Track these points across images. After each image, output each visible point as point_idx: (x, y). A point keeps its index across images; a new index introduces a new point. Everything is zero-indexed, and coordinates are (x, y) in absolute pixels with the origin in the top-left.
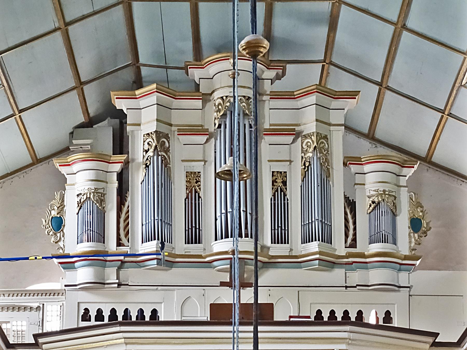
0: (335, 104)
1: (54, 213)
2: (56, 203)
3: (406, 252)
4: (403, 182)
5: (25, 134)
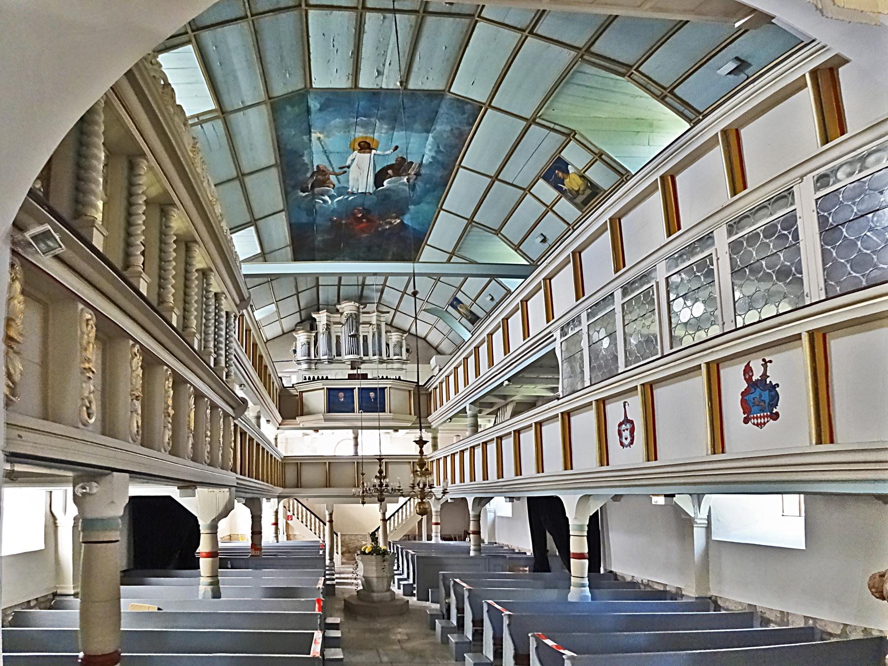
0: (383, 315)
1: (294, 348)
2: (294, 345)
3: (405, 359)
4: (404, 338)
5: (281, 326)
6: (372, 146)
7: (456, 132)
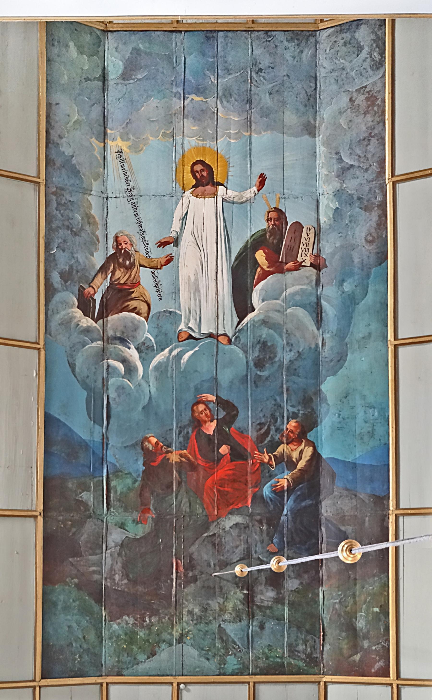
6: (218, 178)
7: (360, 99)
